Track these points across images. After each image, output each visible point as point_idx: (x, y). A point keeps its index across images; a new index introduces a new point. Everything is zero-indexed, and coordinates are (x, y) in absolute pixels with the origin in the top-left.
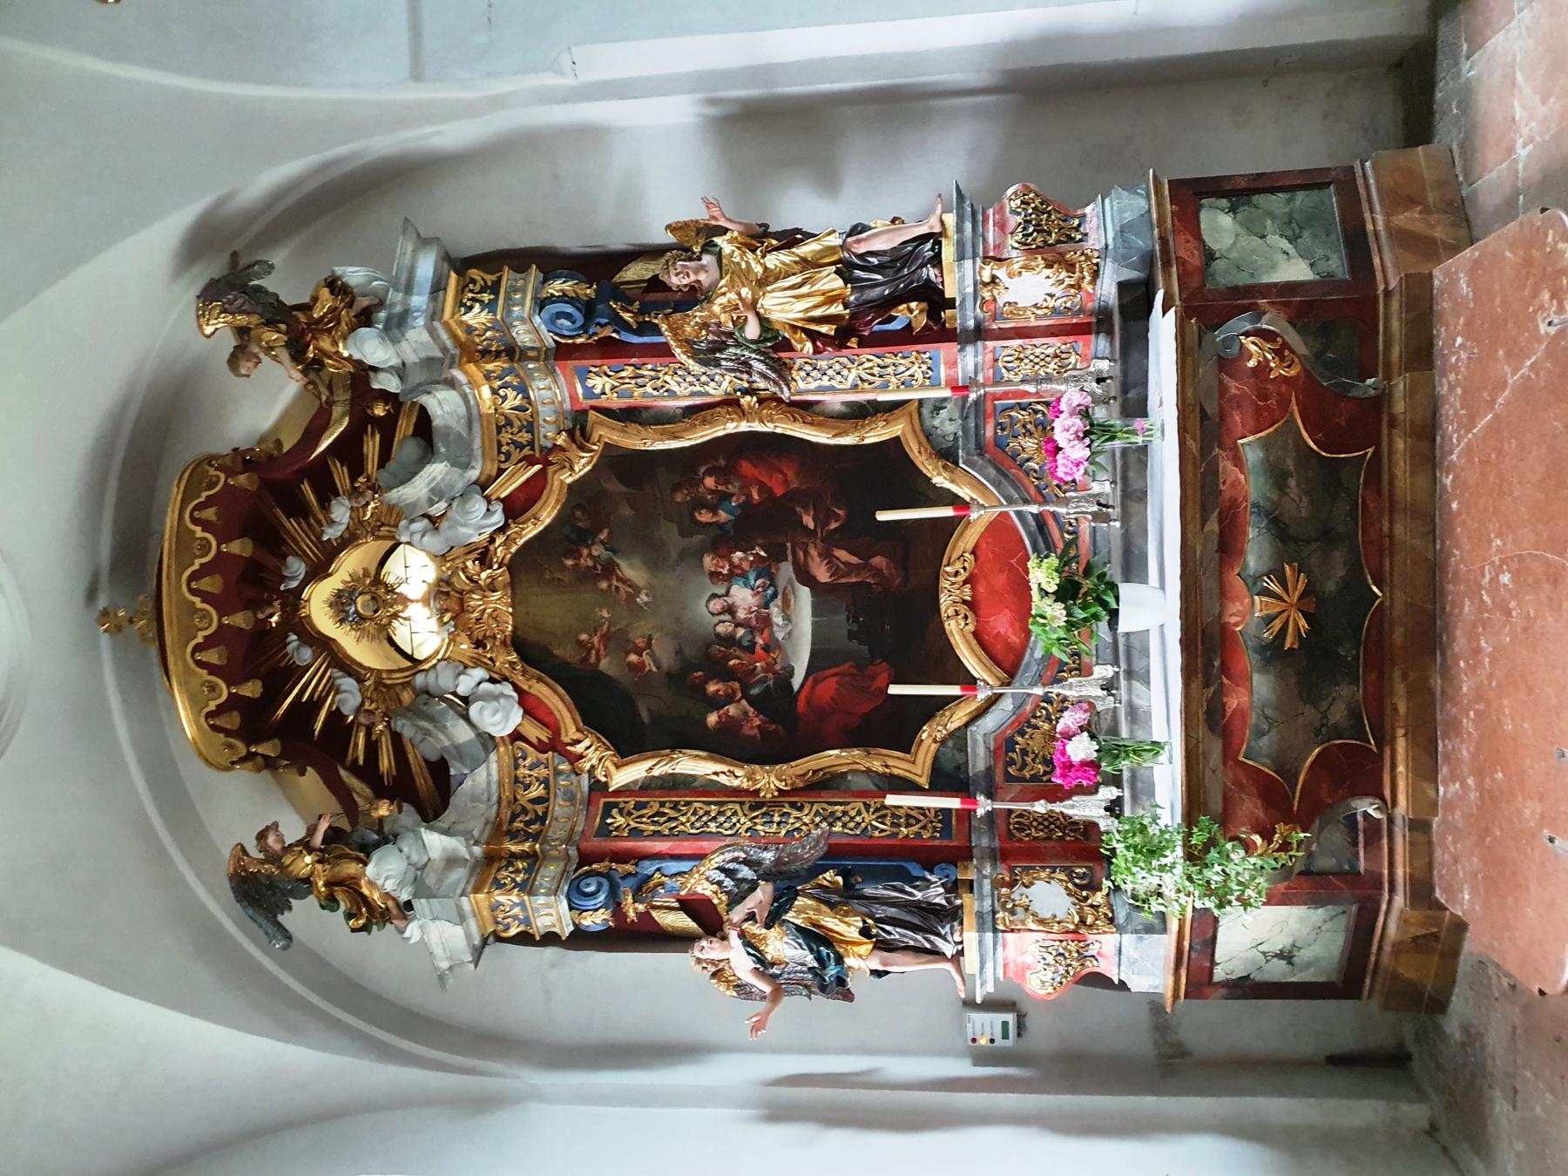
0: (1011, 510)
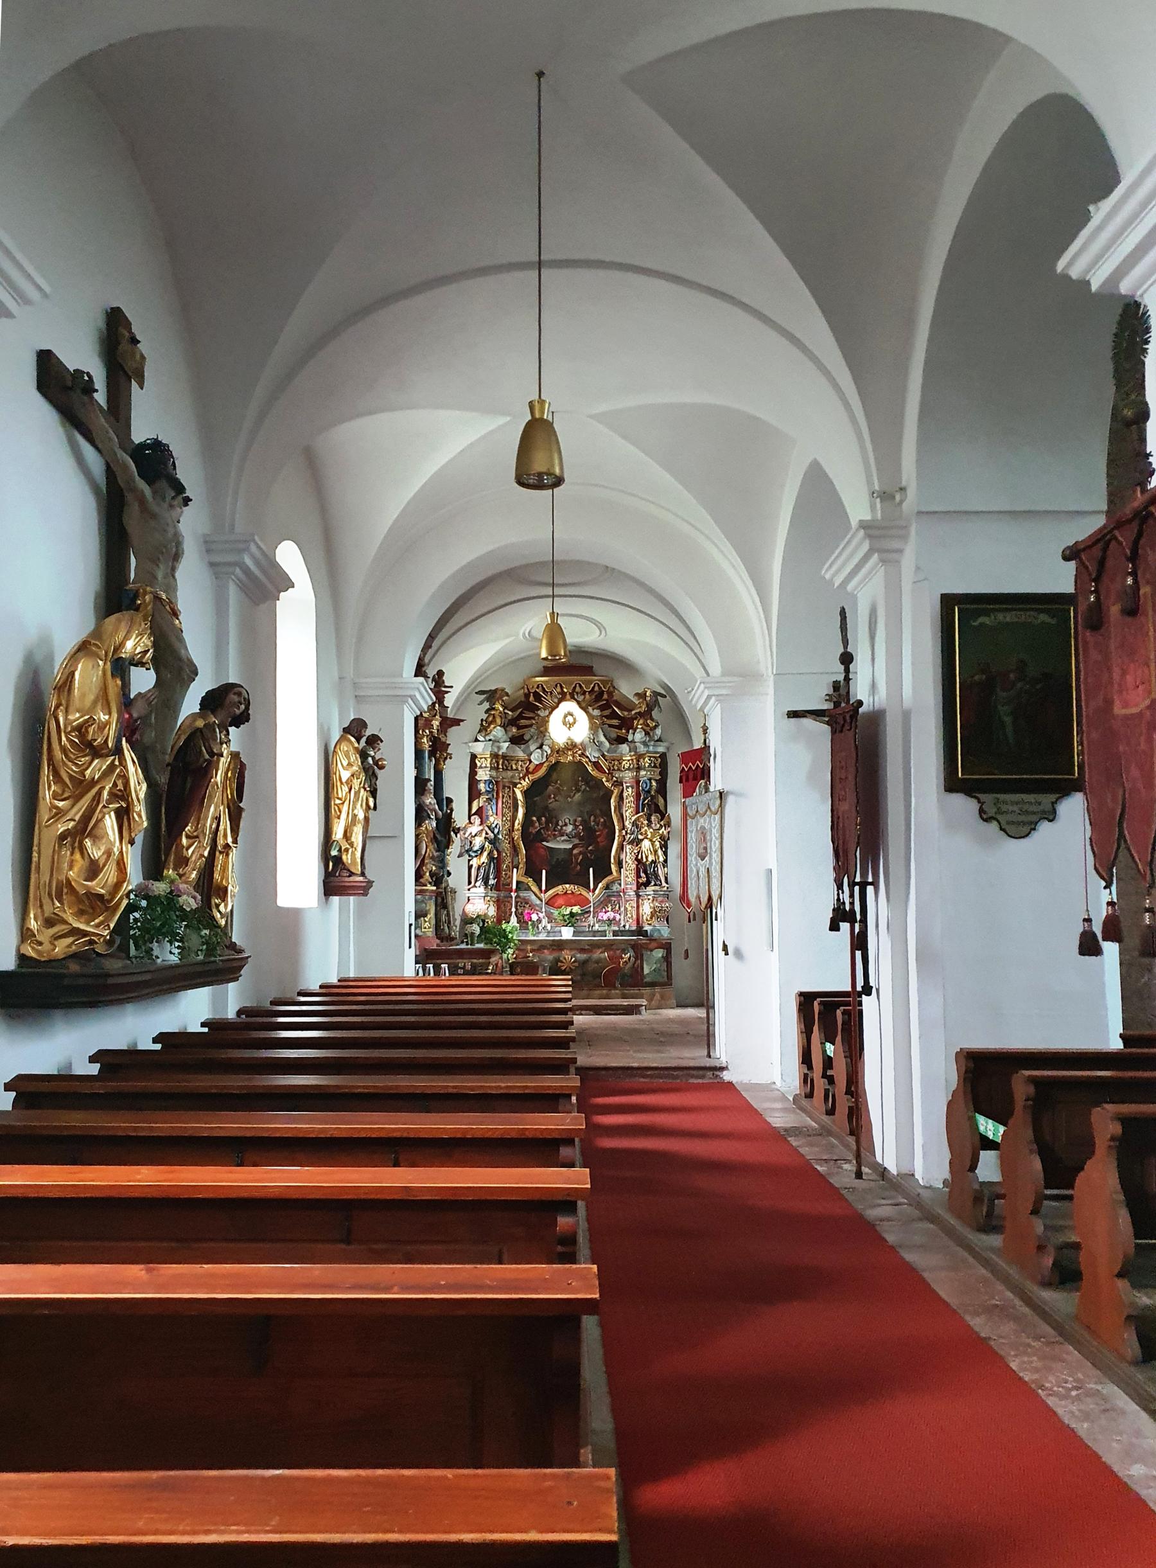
0: (592, 904)
